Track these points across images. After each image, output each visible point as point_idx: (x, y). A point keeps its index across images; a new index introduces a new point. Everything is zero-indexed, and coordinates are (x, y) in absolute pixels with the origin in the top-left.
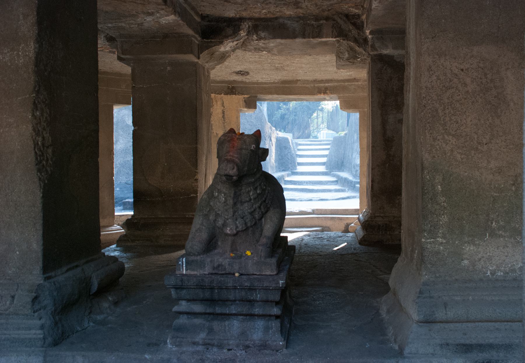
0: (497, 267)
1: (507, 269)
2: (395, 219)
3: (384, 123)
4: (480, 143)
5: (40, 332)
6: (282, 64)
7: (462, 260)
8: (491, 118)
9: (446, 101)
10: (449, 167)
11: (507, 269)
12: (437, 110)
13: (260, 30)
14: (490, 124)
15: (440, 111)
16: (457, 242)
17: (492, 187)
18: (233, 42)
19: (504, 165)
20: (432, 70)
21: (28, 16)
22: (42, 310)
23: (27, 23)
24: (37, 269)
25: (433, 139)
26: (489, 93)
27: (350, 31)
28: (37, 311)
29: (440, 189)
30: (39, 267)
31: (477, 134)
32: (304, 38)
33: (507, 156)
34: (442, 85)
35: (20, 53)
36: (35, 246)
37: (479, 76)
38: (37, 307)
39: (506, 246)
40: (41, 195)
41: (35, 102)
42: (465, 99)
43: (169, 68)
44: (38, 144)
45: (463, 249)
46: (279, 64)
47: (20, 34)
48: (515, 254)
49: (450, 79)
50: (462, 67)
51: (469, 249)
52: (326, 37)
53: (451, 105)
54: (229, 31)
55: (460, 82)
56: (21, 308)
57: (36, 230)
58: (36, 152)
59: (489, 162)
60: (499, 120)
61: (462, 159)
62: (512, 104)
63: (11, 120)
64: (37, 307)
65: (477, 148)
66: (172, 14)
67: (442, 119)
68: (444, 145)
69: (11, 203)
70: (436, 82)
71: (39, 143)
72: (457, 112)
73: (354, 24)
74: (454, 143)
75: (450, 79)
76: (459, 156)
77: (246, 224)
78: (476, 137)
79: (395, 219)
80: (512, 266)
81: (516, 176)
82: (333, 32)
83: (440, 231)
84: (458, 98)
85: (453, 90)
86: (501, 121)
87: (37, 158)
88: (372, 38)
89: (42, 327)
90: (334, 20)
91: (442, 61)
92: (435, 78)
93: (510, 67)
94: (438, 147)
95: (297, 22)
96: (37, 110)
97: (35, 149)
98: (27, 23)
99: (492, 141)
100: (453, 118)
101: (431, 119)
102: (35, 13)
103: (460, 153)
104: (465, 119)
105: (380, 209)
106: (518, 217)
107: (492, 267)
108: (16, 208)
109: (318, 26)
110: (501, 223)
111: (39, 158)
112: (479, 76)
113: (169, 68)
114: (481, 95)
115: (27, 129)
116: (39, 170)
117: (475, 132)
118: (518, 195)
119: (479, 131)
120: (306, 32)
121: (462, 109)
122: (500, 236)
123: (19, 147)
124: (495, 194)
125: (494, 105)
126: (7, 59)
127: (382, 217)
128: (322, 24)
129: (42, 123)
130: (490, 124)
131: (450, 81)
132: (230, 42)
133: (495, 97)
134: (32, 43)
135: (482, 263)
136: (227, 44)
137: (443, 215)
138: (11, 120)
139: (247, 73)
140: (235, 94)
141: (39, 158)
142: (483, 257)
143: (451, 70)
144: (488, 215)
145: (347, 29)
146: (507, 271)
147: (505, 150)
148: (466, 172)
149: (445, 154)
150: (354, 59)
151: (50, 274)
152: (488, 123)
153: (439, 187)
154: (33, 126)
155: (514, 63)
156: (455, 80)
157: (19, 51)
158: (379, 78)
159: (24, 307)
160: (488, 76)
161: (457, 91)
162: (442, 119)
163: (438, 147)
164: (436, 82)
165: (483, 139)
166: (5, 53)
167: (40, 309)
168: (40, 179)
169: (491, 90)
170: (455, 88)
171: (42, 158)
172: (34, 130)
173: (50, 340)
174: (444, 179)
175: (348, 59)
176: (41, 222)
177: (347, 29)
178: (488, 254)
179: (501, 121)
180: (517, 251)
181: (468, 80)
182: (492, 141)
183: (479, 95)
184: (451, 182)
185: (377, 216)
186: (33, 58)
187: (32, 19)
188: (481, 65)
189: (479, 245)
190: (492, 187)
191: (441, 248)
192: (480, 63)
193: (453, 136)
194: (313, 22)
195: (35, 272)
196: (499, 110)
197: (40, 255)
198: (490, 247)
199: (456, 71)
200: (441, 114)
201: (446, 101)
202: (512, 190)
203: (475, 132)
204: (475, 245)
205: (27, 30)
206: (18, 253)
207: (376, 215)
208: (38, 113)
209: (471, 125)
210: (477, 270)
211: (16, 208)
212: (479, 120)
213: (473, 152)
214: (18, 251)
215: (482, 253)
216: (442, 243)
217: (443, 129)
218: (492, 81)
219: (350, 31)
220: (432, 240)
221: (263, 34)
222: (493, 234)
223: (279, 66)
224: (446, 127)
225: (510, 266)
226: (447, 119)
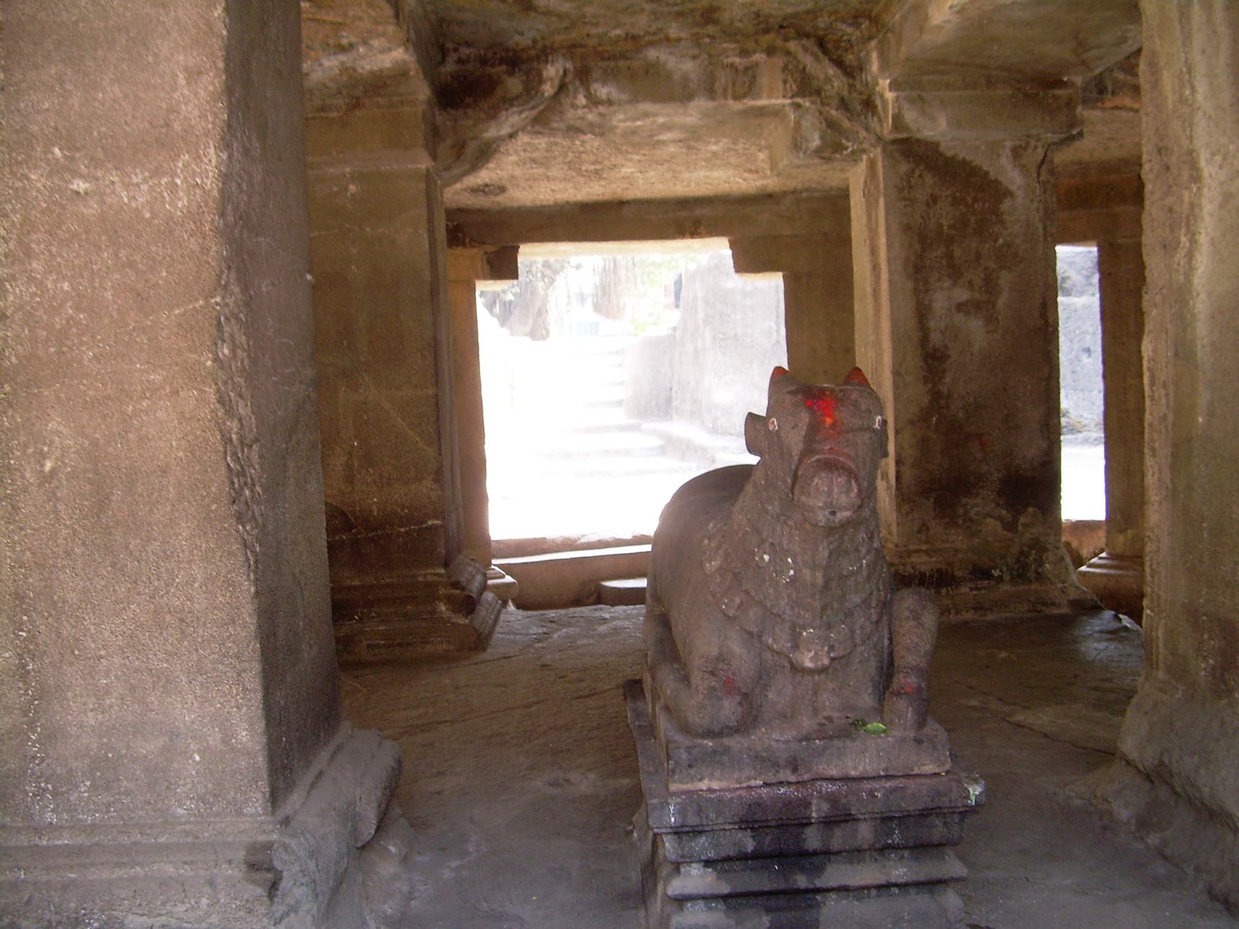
2: (960, 556)
3: (922, 313)
6: (600, 163)
13: (597, 80)
18: (521, 112)
21: (200, 73)
22: (292, 915)
23: (196, 94)
24: (256, 804)
27: (828, 80)
28: (281, 919)
30: (259, 796)
32: (713, 99)
35: (178, 182)
36: (244, 736)
38: (279, 909)
40: (253, 589)
43: (352, 188)
46: (593, 163)
47: (177, 126)
52: (769, 97)
54: (514, 84)
56: (242, 913)
57: (245, 690)
63: (156, 377)
66: (399, 46)
69: (168, 617)
71: (234, 436)
73: (839, 63)
79: (960, 556)
82: (785, 82)
88: (897, 98)
90: (788, 53)
95: (694, 57)
98: (196, 94)
102: (221, 65)
105: (919, 532)
108: (183, 632)
109: (747, 69)
111: (236, 480)
113: (352, 188)
115: (199, 401)
120: (717, 85)
123: (181, 454)
126: (141, 200)
127: (927, 553)
128: (757, 64)
132: (513, 113)
134: (212, 151)
136: (507, 119)
138: (156, 377)
139: (502, 189)
140: (464, 244)
145: (822, 77)
150: (835, 151)
154: (218, 390)
157: (174, 175)
158: (905, 199)
159: (250, 912)
166: (138, 185)
167: (288, 915)
175: (818, 152)
176: (257, 667)
177: (822, 77)
185: (916, 551)
186: (215, 193)
187: (212, 81)
194: (737, 60)
195: (249, 810)
197: (261, 760)
205: (196, 112)
206: (197, 758)
207: (912, 547)
208: (226, 351)
211: (183, 632)
214: (199, 752)
219: (828, 80)
221: (602, 91)
223: (592, 167)
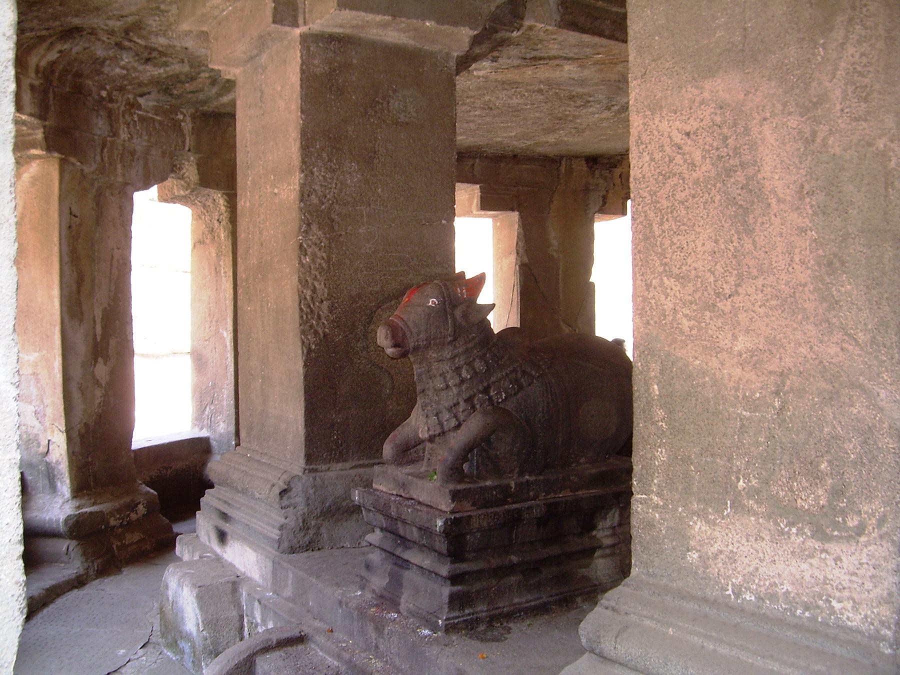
0: (744, 580)
1: (763, 589)
4: (718, 295)
5: (278, 532)
7: (688, 551)
8: (736, 236)
9: (665, 204)
10: (670, 345)
11: (763, 589)
12: (651, 225)
14: (736, 248)
15: (655, 227)
16: (680, 510)
17: (740, 394)
19: (761, 347)
20: (642, 143)
25: (646, 285)
26: (733, 180)
29: (657, 393)
31: (713, 273)
33: (767, 325)
34: (658, 171)
37: (715, 144)
38: (285, 502)
39: (761, 537)
41: (301, 245)
42: (694, 197)
44: (305, 298)
45: (689, 526)
48: (776, 558)
49: (669, 157)
50: (688, 128)
51: (698, 527)
53: (672, 212)
55: (685, 161)
58: (301, 309)
59: (735, 337)
60: (751, 241)
61: (691, 329)
62: (774, 202)
64: (285, 502)
65: (714, 305)
67: (658, 243)
68: (663, 297)
70: (649, 165)
72: (682, 227)
74: (677, 294)
75: (669, 157)
76: (685, 321)
77: (441, 424)
78: (712, 279)
80: (771, 585)
81: (782, 374)
83: (656, 481)
84: (683, 194)
85: (675, 180)
86: (754, 243)
87: (302, 317)
89: (281, 528)
91: (656, 122)
92: (647, 158)
93: (768, 115)
94: (653, 302)
96: (306, 255)
97: (300, 305)
99: (740, 290)
100: (675, 240)
101: (643, 244)
103: (686, 316)
104: (694, 241)
106: (783, 472)
107: (737, 578)
110: (754, 482)
111: (305, 317)
112: (715, 144)
114: (718, 185)
116: (303, 332)
117: (710, 270)
118: (784, 421)
119: (718, 267)
121: (689, 219)
122: (750, 512)
124: (744, 413)
125: (741, 206)
129: (313, 272)
130: (736, 248)
131: (670, 161)
133: (742, 188)
135: (721, 565)
137: (659, 446)
141: (305, 317)
142: (721, 552)
143: (670, 137)
144: (730, 460)
146: (762, 595)
147: (762, 311)
148: (696, 358)
149: (665, 316)
151: (318, 467)
152: (732, 249)
153: (656, 387)
155: (774, 105)
156: (679, 159)
160: (730, 141)
161: (681, 181)
162: (658, 243)
163: (653, 302)
164: (649, 165)
165: (725, 286)
168: (303, 343)
169: (735, 171)
170: (677, 176)
171: (309, 317)
172: (300, 281)
173: (286, 544)
174: (662, 372)
178: (730, 547)
179: (754, 243)
180: (780, 552)
181: (697, 155)
182: (740, 290)
183: (715, 186)
184: (673, 378)
188: (718, 119)
189: (715, 524)
190: (740, 394)
191: (657, 515)
192: (716, 114)
193: (678, 277)
196: (751, 216)
198: (733, 532)
199: (678, 138)
200: (657, 233)
201: (665, 204)
202: (774, 408)
203: (710, 270)
204: (708, 522)
209: (704, 252)
210: (710, 579)
212: (716, 241)
213: (708, 314)
215: (719, 543)
216: (657, 506)
217: (661, 264)
218: (737, 151)
220: (644, 496)
222: (738, 506)
224: (665, 260)
225: (767, 583)
226: (667, 242)
